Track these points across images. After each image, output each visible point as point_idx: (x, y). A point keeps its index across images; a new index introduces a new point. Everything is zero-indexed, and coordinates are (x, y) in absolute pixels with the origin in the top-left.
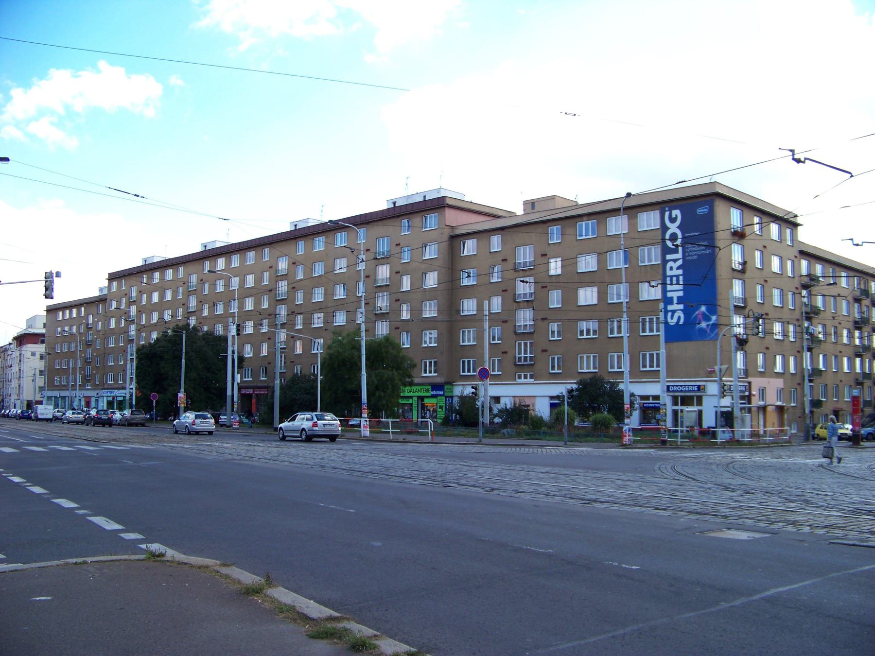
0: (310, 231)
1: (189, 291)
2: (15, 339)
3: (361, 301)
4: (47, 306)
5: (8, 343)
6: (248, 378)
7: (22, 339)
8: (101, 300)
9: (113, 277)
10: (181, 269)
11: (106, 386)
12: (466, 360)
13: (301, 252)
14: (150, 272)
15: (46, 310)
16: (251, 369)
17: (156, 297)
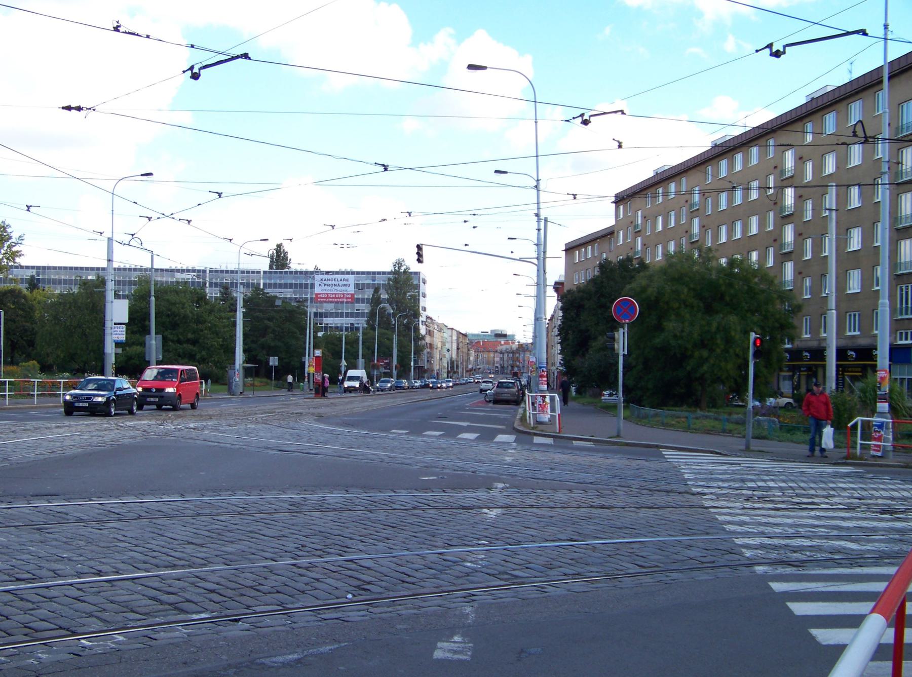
0: (808, 110)
1: (691, 212)
4: (566, 244)
9: (621, 199)
10: (755, 150)
12: (904, 332)
15: (564, 249)
16: (859, 315)
17: (830, 166)
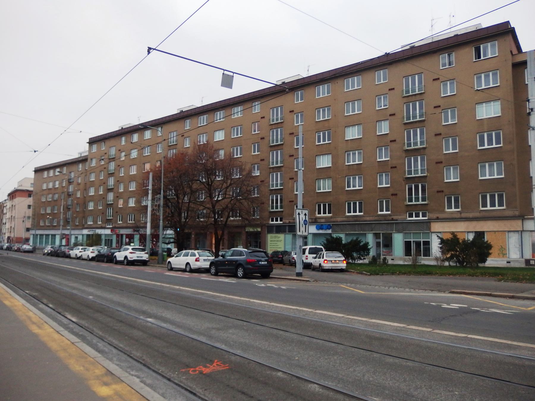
2: (9, 195)
3: (483, 107)
5: (4, 200)
6: (110, 217)
7: (12, 195)
8: (83, 160)
9: (92, 142)
11: (86, 226)
13: (123, 143)
14: (129, 135)
